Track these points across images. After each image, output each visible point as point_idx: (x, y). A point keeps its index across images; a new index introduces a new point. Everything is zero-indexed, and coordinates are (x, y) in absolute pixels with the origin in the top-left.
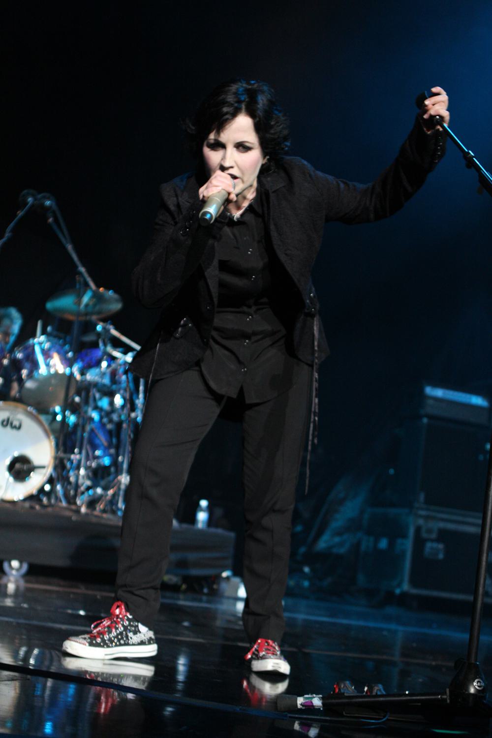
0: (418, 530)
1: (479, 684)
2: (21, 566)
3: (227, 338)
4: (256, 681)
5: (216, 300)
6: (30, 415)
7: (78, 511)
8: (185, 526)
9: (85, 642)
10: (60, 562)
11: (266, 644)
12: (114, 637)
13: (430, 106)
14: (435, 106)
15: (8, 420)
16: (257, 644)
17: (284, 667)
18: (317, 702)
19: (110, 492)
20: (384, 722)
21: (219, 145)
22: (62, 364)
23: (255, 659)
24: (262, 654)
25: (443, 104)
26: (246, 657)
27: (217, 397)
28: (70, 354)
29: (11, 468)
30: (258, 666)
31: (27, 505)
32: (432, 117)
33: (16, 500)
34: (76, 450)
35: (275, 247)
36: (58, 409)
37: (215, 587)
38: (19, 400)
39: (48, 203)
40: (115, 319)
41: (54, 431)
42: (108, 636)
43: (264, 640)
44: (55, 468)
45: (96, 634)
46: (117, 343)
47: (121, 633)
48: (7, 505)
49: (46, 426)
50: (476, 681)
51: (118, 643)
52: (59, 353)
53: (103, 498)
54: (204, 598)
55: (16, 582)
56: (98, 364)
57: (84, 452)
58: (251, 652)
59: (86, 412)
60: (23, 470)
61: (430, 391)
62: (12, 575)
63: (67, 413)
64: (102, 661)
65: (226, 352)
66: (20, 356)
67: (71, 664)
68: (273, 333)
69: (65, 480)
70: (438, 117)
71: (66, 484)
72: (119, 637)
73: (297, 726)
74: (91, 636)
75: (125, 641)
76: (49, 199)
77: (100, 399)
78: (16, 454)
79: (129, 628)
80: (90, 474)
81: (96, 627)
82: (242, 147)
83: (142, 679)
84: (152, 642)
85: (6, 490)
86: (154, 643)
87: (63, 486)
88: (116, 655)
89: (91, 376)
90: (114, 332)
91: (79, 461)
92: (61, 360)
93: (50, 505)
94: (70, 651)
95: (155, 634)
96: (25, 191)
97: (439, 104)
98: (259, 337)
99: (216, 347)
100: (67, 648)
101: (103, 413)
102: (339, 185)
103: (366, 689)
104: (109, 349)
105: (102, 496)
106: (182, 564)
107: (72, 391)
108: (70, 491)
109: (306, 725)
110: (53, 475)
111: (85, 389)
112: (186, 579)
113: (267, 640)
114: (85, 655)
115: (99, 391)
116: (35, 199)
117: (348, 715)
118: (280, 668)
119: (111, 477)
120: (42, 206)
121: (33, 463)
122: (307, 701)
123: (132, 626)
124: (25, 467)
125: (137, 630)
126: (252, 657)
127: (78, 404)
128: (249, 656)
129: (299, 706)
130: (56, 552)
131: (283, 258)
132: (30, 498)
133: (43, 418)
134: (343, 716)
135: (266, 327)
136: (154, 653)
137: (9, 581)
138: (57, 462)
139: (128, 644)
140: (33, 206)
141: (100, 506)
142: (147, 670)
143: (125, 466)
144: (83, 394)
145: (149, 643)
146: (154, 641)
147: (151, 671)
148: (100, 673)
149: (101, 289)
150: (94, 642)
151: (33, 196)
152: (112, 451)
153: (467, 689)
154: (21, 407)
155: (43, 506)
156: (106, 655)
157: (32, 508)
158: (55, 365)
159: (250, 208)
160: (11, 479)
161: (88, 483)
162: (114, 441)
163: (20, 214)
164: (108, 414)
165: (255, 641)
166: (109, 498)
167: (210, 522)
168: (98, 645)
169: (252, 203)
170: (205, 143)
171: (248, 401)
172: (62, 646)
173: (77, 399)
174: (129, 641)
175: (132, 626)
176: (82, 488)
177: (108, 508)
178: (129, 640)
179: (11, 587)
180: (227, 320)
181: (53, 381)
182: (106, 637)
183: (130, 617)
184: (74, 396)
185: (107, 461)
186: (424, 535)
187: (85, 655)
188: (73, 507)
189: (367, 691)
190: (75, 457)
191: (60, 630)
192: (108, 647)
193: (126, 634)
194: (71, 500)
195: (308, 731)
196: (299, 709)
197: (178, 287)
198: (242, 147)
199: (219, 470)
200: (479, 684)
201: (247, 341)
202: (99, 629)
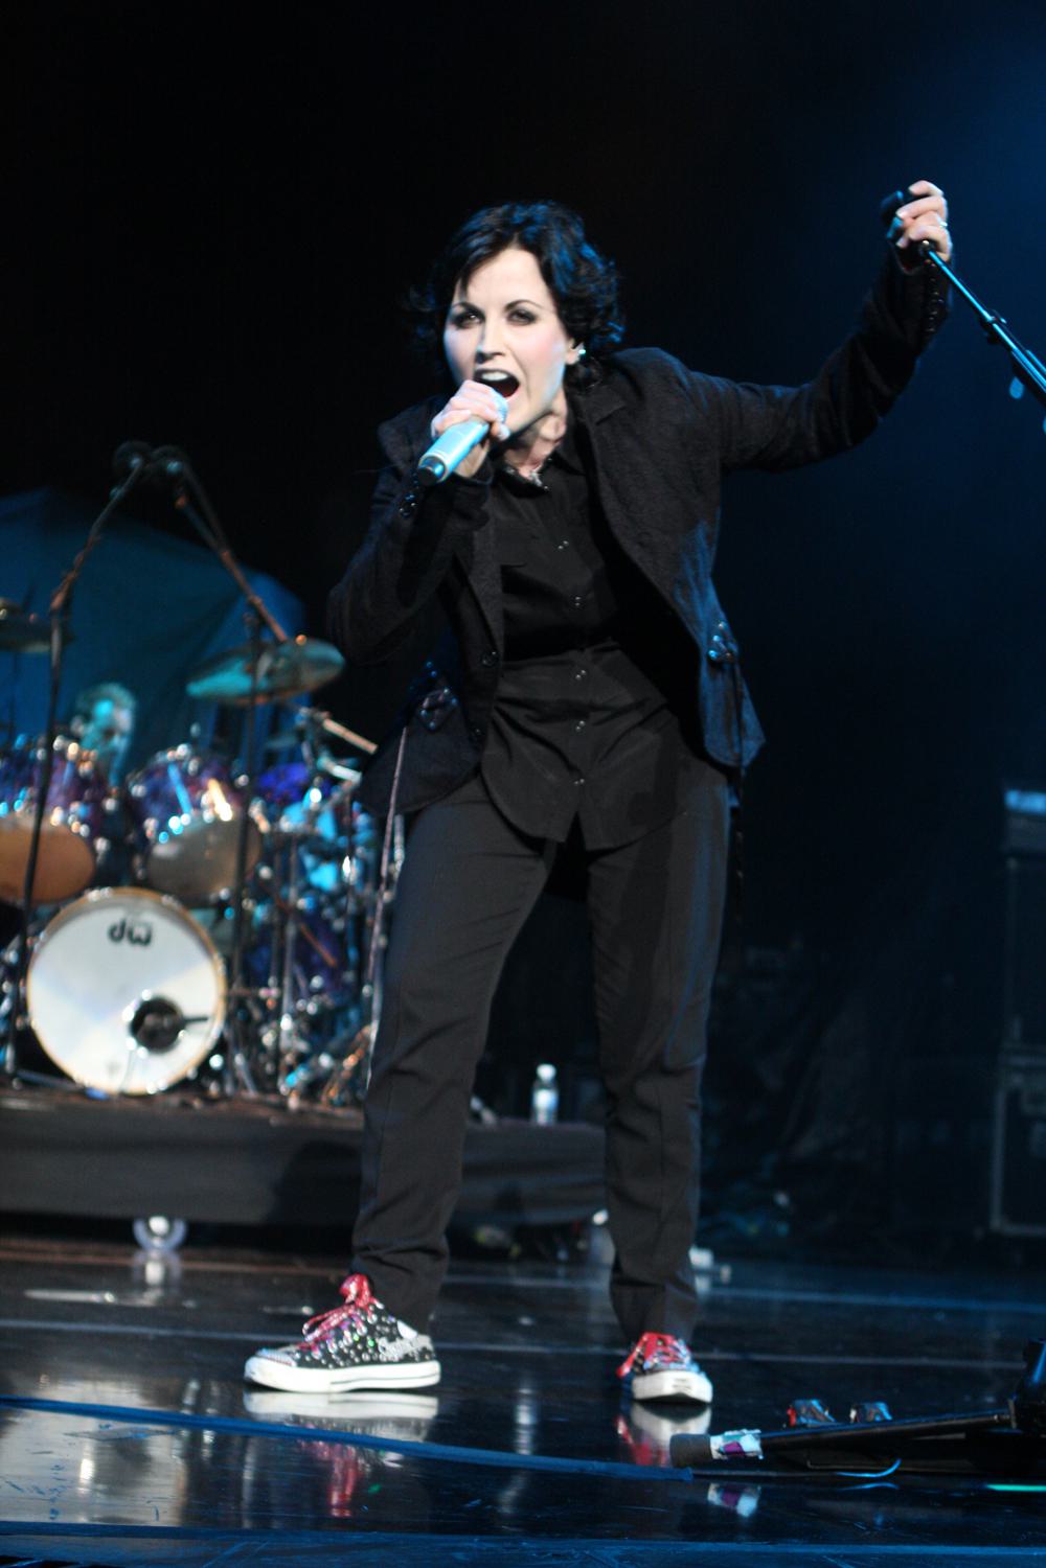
0: (1014, 1098)
2: (171, 1229)
3: (544, 719)
4: (643, 1418)
5: (500, 644)
6: (167, 912)
7: (282, 1106)
8: (509, 1122)
9: (288, 1359)
10: (252, 1213)
11: (660, 1343)
12: (349, 1348)
13: (909, 221)
14: (919, 219)
16: (641, 1343)
17: (700, 1387)
18: (750, 1442)
19: (350, 1062)
20: (889, 1476)
21: (473, 315)
22: (229, 801)
23: (638, 1375)
24: (648, 1364)
25: (936, 216)
26: (620, 1371)
27: (536, 845)
28: (242, 780)
29: (136, 1027)
30: (645, 1387)
31: (174, 1100)
32: (914, 245)
33: (151, 1090)
34: (271, 981)
35: (617, 531)
37: (581, 1245)
38: (146, 884)
39: (173, 466)
40: (324, 699)
41: (219, 943)
42: (335, 1346)
43: (655, 1336)
44: (229, 1019)
45: (311, 1344)
46: (340, 750)
47: (363, 1340)
48: (134, 1104)
49: (205, 934)
51: (357, 1360)
52: (219, 778)
53: (335, 1075)
55: (163, 1260)
56: (302, 792)
57: (287, 982)
58: (630, 1360)
60: (163, 1030)
61: (1013, 799)
62: (153, 1247)
63: (248, 904)
64: (326, 1398)
65: (540, 748)
66: (138, 790)
67: (261, 1406)
68: (638, 705)
70: (926, 242)
71: (254, 1050)
72: (359, 1347)
73: (713, 1496)
74: (302, 1348)
75: (371, 1355)
76: (174, 457)
77: (316, 868)
78: (147, 996)
79: (378, 1328)
80: (304, 1026)
81: (310, 1331)
82: (519, 315)
83: (413, 1423)
84: (427, 1357)
85: (129, 1074)
86: (431, 1359)
87: (248, 1058)
88: (356, 1382)
89: (291, 821)
90: (332, 727)
91: (279, 1001)
92: (226, 793)
93: (223, 1097)
94: (259, 1378)
95: (434, 1340)
96: (124, 446)
97: (926, 216)
98: (605, 714)
99: (515, 738)
100: (253, 1373)
101: (323, 899)
102: (736, 391)
103: (853, 1414)
104: (325, 762)
106: (509, 1202)
107: (254, 855)
108: (264, 1064)
109: (732, 1491)
110: (226, 1034)
111: (281, 849)
112: (522, 1233)
113: (662, 1336)
114: (292, 1386)
115: (312, 852)
117: (818, 1467)
118: (689, 1388)
120: (162, 473)
121: (180, 1011)
122: (730, 1442)
123: (385, 1324)
124: (166, 1022)
125: (394, 1332)
126: (632, 1370)
127: (267, 882)
128: (626, 1369)
129: (716, 1455)
130: (244, 1195)
131: (635, 553)
132: (182, 1085)
133: (196, 916)
134: (805, 1468)
135: (626, 698)
136: (434, 1380)
137: (147, 1259)
138: (232, 1006)
139: (378, 1362)
140: (142, 474)
141: (332, 1093)
142: (422, 1406)
143: (376, 1006)
144: (278, 859)
146: (434, 1355)
147: (431, 1407)
148: (324, 1421)
149: (300, 638)
150: (308, 1358)
154: (147, 899)
155: (209, 1101)
156: (333, 1383)
157: (186, 1105)
158: (212, 805)
159: (554, 462)
160: (143, 1051)
161: (302, 1046)
162: (352, 954)
163: (117, 493)
164: (333, 898)
165: (637, 1340)
166: (345, 1074)
167: (563, 1110)
168: (315, 1364)
169: (557, 448)
171: (590, 846)
172: (242, 1369)
173: (265, 872)
174: (381, 1357)
175: (385, 1324)
176: (289, 1059)
177: (346, 1096)
178: (379, 1353)
179: (154, 1272)
180: (540, 681)
181: (212, 838)
182: (333, 1348)
183: (380, 1306)
184: (259, 864)
186: (1027, 1108)
187: (292, 1386)
188: (272, 1099)
189: (856, 1418)
190: (269, 993)
191: (248, 1343)
192: (337, 1366)
195: (736, 1503)
196: (716, 1460)
197: (432, 627)
198: (519, 315)
199: (550, 997)
201: (582, 722)
202: (317, 1333)
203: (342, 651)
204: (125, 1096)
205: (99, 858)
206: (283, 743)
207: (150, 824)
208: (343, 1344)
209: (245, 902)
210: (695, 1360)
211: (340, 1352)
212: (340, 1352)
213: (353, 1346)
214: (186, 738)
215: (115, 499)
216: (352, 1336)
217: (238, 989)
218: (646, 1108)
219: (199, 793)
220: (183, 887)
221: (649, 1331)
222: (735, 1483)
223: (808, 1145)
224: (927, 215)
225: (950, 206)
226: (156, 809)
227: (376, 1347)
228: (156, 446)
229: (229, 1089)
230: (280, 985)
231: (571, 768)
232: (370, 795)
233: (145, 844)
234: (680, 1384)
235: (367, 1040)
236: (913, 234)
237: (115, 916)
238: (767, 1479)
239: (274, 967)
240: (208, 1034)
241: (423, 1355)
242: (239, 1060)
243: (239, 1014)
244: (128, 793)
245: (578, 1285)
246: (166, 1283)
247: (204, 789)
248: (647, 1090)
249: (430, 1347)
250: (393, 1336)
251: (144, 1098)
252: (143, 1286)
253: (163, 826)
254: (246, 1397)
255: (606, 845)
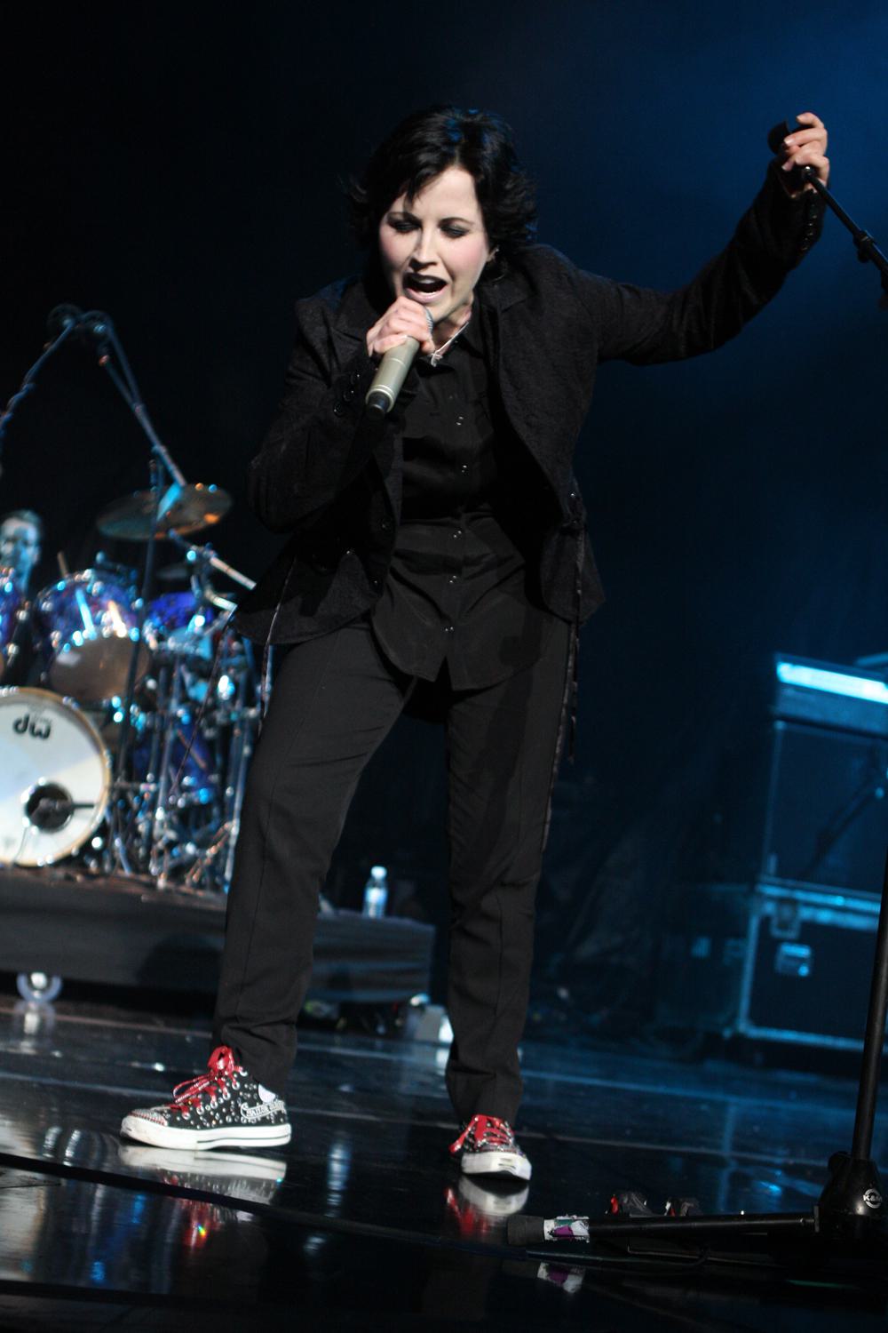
0: (765, 922)
1: (872, 1198)
6: (65, 711)
7: (152, 886)
9: (161, 1118)
10: (118, 975)
11: (489, 1125)
12: (215, 1111)
13: (795, 148)
14: (803, 147)
15: (27, 719)
16: (472, 1124)
17: (521, 1166)
18: (579, 1228)
19: (211, 852)
21: (411, 224)
22: (124, 621)
23: (468, 1151)
25: (817, 144)
27: (400, 679)
29: (31, 808)
30: (474, 1163)
32: (798, 168)
33: (40, 864)
36: (116, 701)
37: (398, 1022)
39: (99, 328)
41: (109, 742)
42: (202, 1109)
44: (111, 807)
46: (222, 584)
47: (227, 1104)
48: (26, 874)
50: (868, 1192)
52: (117, 600)
53: (198, 862)
54: (379, 1043)
55: (40, 1011)
56: (187, 619)
57: (163, 779)
58: (462, 1138)
59: (167, 707)
61: (790, 673)
65: (416, 597)
66: (46, 606)
67: (137, 1159)
69: (130, 830)
73: (542, 1273)
75: (233, 1118)
76: (101, 321)
77: (194, 684)
78: (42, 782)
79: (241, 1094)
80: (175, 819)
81: (180, 1093)
82: (449, 228)
86: (285, 1122)
87: (124, 841)
88: (216, 1143)
90: (216, 563)
91: (156, 794)
92: (122, 614)
94: (134, 1134)
95: (288, 1105)
105: (193, 865)
106: (339, 981)
107: (143, 669)
108: (138, 849)
110: (108, 820)
111: (163, 665)
112: (347, 1009)
114: (163, 1143)
116: (77, 322)
119: (212, 826)
120: (89, 333)
123: (247, 1091)
124: (57, 806)
125: (255, 1098)
126: (462, 1147)
127: (152, 692)
129: (547, 1236)
130: (112, 958)
132: (66, 861)
134: (626, 1255)
136: (285, 1141)
137: (27, 1010)
138: (115, 797)
140: (72, 333)
141: (193, 877)
142: (274, 1169)
143: (237, 805)
144: (162, 674)
145: (278, 1122)
146: (287, 1118)
147: (280, 1170)
151: (73, 315)
152: (214, 778)
153: (852, 1208)
156: (199, 1142)
157: (69, 878)
158: (111, 623)
160: (35, 829)
161: (171, 835)
162: (219, 760)
163: (50, 347)
166: (207, 862)
167: (390, 906)
168: (184, 1125)
170: (385, 218)
171: (456, 687)
172: (120, 1126)
173: (151, 684)
174: (242, 1119)
175: (247, 1091)
178: (241, 1116)
179: (31, 1021)
180: (420, 538)
182: (200, 1110)
183: (244, 1074)
185: (203, 796)
186: (776, 932)
187: (163, 1143)
188: (144, 878)
189: (670, 1208)
192: (203, 1127)
193: (236, 1105)
194: (139, 866)
198: (449, 228)
199: (403, 809)
200: (872, 1198)
203: (56, 555)
204: (17, 866)
205: (9, 661)
206: (176, 573)
207: (56, 636)
208: (208, 1108)
209: (132, 708)
210: (518, 1141)
211: (206, 1115)
212: (206, 1115)
213: (218, 1110)
214: (90, 564)
215: (48, 351)
216: (218, 1101)
217: (121, 782)
218: (487, 917)
219: (99, 613)
220: (82, 691)
221: (480, 1114)
222: (565, 1264)
223: (588, 949)
224: (812, 143)
225: (830, 137)
226: (60, 622)
227: (237, 1110)
228: (85, 310)
229: (107, 867)
230: (156, 781)
231: (441, 615)
232: (239, 625)
233: (49, 652)
234: (506, 1163)
235: (227, 834)
236: (798, 159)
237: (20, 712)
238: (595, 1263)
239: (152, 765)
240: (94, 818)
241: (278, 1119)
242: (117, 843)
243: (120, 803)
244: (39, 606)
245: (394, 1058)
246: (40, 1034)
247: (105, 609)
248: (488, 903)
249: (284, 1111)
250: (255, 1101)
251: (34, 869)
252: (21, 1035)
253: (66, 638)
254: (121, 1149)
255: (469, 686)
